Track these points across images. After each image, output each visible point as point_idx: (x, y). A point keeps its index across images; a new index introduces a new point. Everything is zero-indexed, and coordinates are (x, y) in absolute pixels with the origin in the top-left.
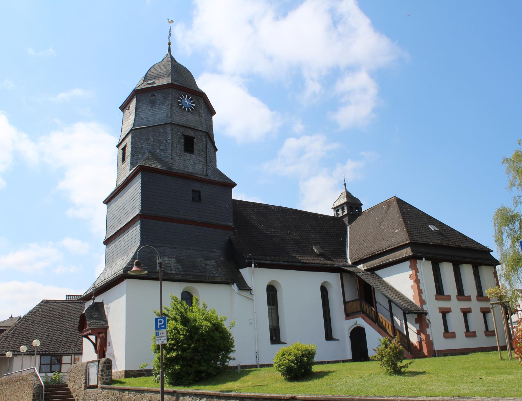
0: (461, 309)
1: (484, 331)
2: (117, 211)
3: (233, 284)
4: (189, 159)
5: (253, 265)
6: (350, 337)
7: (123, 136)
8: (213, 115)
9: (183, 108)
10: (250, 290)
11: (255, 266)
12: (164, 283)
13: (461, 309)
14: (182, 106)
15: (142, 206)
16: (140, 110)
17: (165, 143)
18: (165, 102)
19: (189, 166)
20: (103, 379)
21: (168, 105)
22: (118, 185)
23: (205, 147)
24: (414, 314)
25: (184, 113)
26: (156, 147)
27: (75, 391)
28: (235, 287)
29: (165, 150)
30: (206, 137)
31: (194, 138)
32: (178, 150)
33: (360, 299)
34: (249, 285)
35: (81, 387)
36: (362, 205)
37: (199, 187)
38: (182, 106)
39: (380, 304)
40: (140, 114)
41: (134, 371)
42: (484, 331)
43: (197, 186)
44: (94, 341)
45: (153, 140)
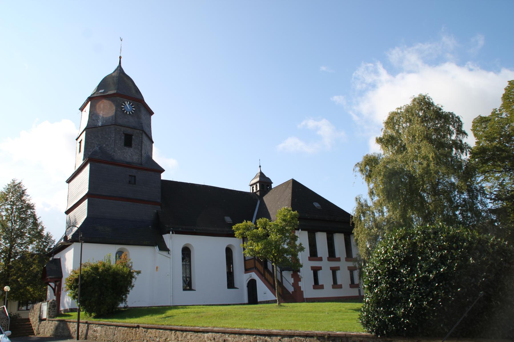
3: (156, 246)
5: (171, 232)
6: (247, 286)
10: (167, 250)
11: (173, 233)
14: (125, 110)
15: (89, 188)
27: (33, 323)
31: (133, 135)
32: (119, 145)
34: (168, 247)
35: (37, 320)
36: (272, 183)
38: (125, 110)
43: (134, 172)
44: (54, 287)
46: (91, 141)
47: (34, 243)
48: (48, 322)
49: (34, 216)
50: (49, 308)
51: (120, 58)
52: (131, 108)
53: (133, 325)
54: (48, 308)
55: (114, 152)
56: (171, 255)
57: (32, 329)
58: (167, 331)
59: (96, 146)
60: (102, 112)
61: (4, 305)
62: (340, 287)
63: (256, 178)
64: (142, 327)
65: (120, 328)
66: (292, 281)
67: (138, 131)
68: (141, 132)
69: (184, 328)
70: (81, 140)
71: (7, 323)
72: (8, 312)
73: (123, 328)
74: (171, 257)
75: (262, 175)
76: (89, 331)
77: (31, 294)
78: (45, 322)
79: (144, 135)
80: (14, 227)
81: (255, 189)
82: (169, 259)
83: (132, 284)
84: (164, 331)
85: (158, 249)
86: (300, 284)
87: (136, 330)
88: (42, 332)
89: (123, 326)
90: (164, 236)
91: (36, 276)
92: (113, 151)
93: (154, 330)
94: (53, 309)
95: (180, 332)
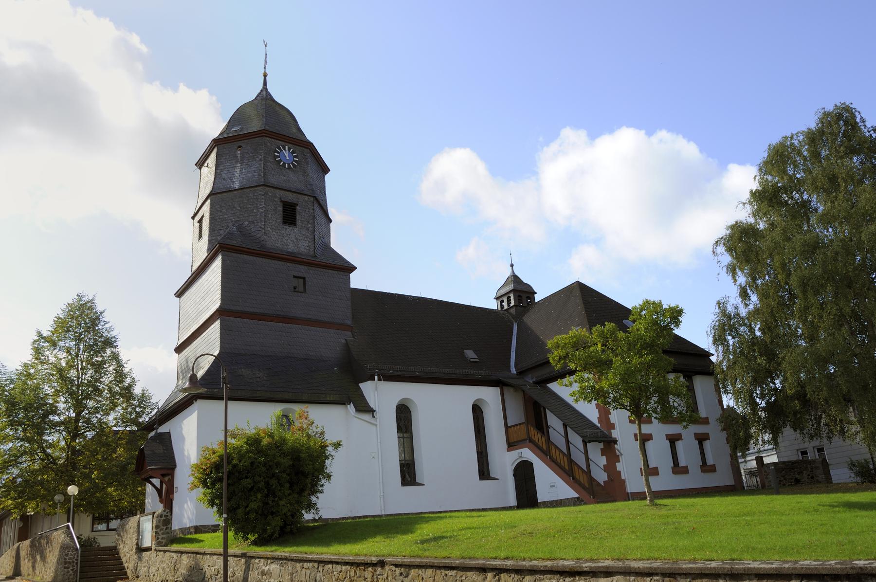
0: (666, 435)
1: (700, 465)
2: (192, 306)
4: (290, 235)
5: (376, 377)
7: (200, 204)
8: (326, 174)
9: (281, 164)
10: (371, 411)
11: (379, 379)
12: (229, 402)
13: (667, 435)
14: (280, 161)
15: (222, 299)
16: (222, 168)
17: (255, 213)
18: (256, 157)
19: (290, 243)
20: (158, 538)
21: (261, 160)
22: (193, 271)
23: (312, 217)
24: (597, 443)
25: (283, 171)
26: (244, 219)
27: (125, 556)
28: (351, 408)
29: (256, 222)
30: (314, 204)
32: (274, 223)
33: (527, 422)
34: (372, 405)
35: (132, 549)
36: (536, 293)
37: (303, 272)
38: (280, 161)
39: (554, 429)
40: (222, 173)
41: (208, 526)
42: (700, 465)
43: (302, 270)
44: (159, 486)
45: (239, 209)
46: (221, 217)
47: (119, 408)
48: (155, 555)
49: (115, 357)
50: (157, 527)
51: (265, 76)
52: (291, 162)
53: (368, 559)
54: (154, 525)
55: (265, 234)
56: (378, 420)
57: (124, 568)
58: (470, 574)
59: (230, 224)
60: (239, 165)
61: (68, 521)
62: (685, 471)
63: (507, 285)
64: (392, 565)
65: (330, 566)
66: (603, 461)
67: (306, 198)
68: (312, 199)
69: (527, 564)
70: (203, 216)
71: (76, 556)
72: (76, 535)
73: (339, 567)
74: (378, 423)
75: (515, 279)
76: (250, 572)
77: (114, 501)
78: (149, 553)
79: (316, 205)
80: (82, 379)
81: (505, 304)
82: (373, 428)
83: (327, 471)
84: (460, 573)
85: (354, 409)
86: (619, 466)
87: (375, 571)
88: (144, 574)
89: (337, 563)
90: (363, 386)
91: (124, 468)
92: (263, 231)
93: (429, 572)
94: (165, 527)
95: (513, 575)
